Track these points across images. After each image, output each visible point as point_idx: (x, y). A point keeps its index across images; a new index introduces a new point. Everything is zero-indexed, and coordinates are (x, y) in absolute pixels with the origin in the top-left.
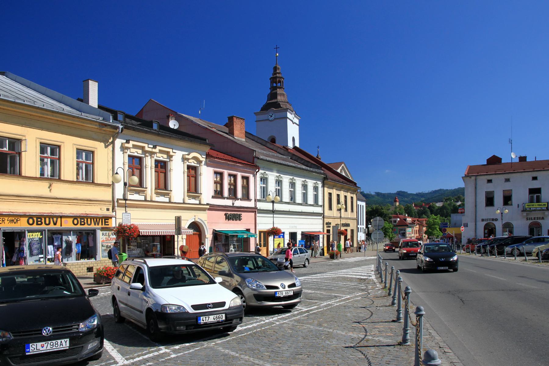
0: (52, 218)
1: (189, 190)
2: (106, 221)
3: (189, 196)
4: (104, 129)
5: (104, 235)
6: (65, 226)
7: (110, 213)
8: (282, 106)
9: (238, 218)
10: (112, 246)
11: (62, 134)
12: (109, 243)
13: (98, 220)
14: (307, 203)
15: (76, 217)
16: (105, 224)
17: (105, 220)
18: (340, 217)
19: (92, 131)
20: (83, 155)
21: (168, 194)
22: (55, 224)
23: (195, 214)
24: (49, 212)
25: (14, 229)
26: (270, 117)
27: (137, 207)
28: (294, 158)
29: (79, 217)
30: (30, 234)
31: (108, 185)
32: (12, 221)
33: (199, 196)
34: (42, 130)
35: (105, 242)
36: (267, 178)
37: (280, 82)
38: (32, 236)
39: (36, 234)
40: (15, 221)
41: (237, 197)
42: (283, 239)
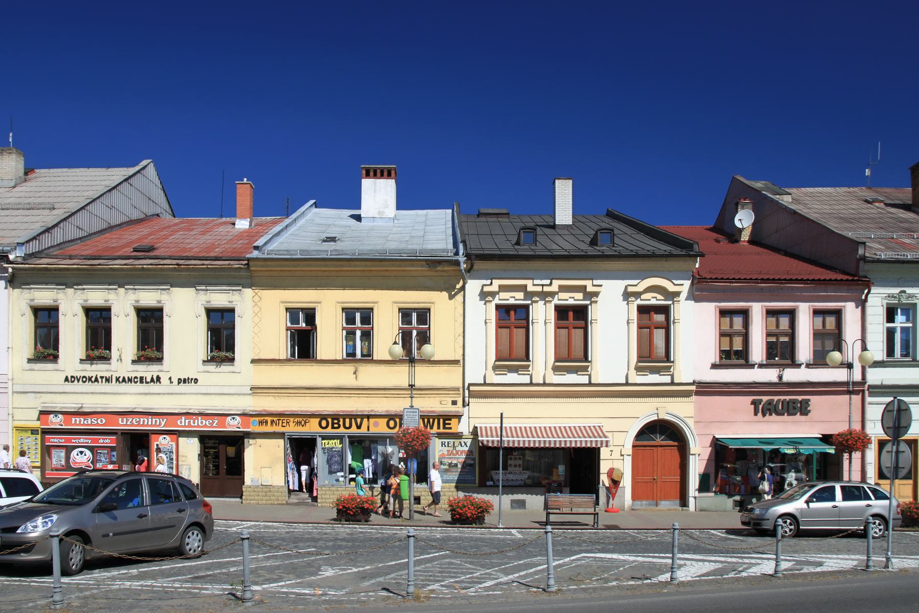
0: (354, 419)
1: (650, 357)
2: (447, 422)
3: (638, 369)
4: (439, 268)
5: (445, 446)
6: (373, 430)
7: (458, 408)
9: (795, 408)
10: (459, 464)
11: (375, 290)
13: (431, 420)
15: (393, 417)
16: (444, 428)
19: (424, 276)
21: (585, 369)
22: (359, 427)
23: (658, 405)
24: (355, 409)
25: (301, 434)
27: (513, 397)
30: (325, 441)
31: (456, 362)
32: (299, 423)
33: (670, 367)
34: (344, 290)
38: (328, 444)
39: (334, 441)
40: (303, 422)
41: (795, 361)
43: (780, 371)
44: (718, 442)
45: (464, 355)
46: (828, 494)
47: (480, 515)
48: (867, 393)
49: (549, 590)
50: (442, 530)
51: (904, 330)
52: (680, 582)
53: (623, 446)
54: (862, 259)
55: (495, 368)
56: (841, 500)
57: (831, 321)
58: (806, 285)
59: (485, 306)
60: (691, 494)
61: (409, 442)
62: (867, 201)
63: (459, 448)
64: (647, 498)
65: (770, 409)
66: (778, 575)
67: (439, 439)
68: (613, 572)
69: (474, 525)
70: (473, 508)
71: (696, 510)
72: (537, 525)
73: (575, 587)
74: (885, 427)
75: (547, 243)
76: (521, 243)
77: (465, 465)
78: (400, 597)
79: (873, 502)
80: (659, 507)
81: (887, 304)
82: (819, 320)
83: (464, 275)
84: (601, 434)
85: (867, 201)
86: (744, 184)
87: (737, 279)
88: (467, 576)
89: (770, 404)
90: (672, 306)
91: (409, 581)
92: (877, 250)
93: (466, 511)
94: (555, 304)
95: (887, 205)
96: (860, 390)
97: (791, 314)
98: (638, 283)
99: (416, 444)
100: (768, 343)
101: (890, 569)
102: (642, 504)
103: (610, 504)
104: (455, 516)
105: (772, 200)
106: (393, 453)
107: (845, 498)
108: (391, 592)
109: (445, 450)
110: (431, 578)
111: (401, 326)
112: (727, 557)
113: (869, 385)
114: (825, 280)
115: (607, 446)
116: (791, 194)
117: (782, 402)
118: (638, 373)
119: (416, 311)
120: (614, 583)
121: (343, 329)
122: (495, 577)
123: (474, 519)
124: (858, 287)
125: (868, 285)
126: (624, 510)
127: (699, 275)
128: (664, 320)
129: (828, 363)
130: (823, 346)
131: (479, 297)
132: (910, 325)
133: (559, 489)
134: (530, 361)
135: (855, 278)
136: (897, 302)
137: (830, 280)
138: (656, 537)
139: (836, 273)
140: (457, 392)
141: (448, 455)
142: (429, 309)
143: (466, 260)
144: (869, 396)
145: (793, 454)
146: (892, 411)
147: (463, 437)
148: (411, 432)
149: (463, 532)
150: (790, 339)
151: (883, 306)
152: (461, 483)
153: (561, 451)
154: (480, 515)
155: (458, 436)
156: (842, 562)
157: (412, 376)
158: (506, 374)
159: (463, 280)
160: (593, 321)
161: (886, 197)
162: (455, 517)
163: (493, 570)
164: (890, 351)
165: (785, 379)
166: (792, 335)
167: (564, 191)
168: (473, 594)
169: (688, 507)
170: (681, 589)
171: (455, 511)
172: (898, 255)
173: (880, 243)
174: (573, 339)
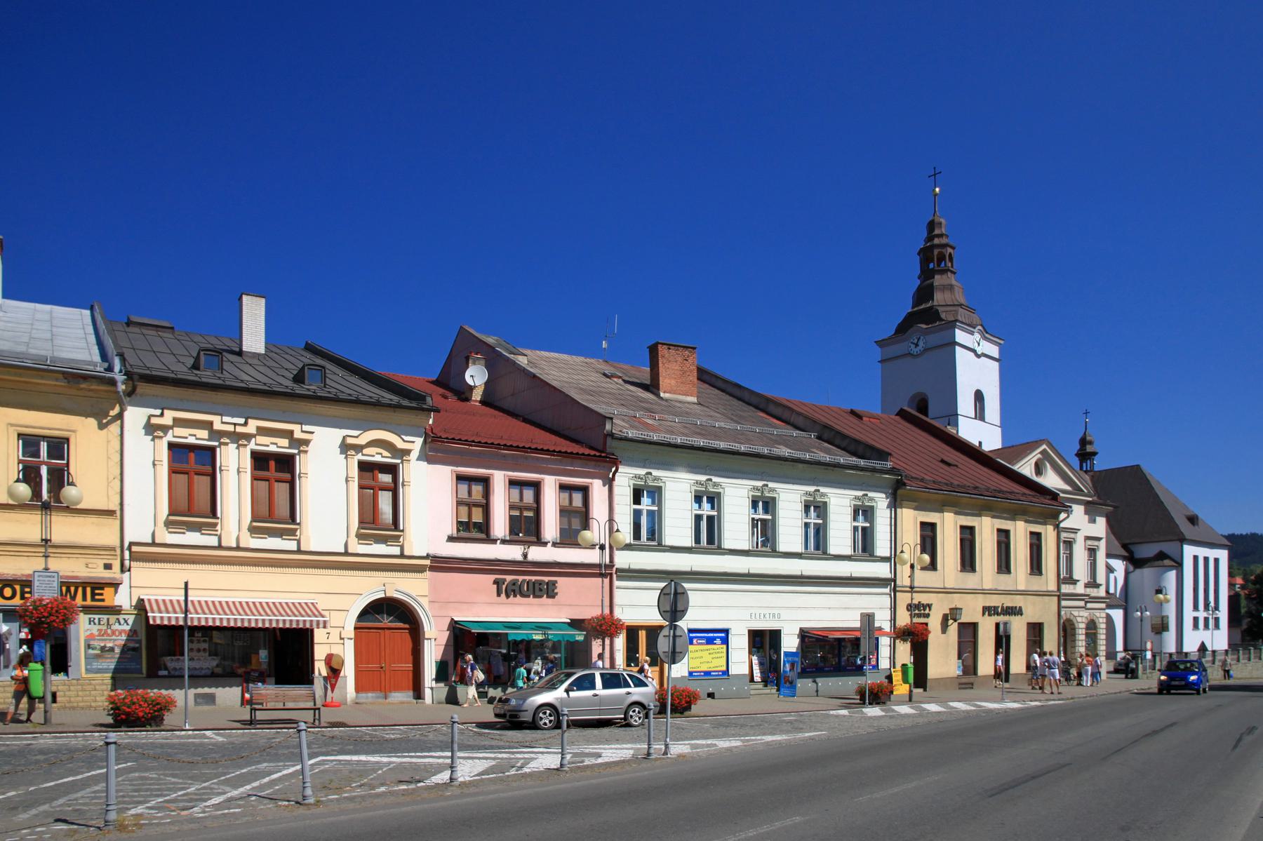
2: (97, 592)
3: (360, 536)
4: (83, 386)
7: (115, 573)
8: (943, 316)
9: (541, 590)
10: (116, 648)
12: (108, 641)
13: (73, 589)
14: (825, 553)
16: (93, 599)
17: (93, 590)
18: (912, 587)
20: (42, 446)
23: (386, 580)
26: (913, 346)
28: (826, 436)
29: (16, 581)
31: (110, 513)
33: (400, 536)
35: (98, 639)
36: (660, 488)
37: (941, 258)
41: (541, 539)
42: (725, 646)
43: (525, 549)
44: (458, 626)
45: (122, 504)
46: (586, 683)
47: (156, 713)
48: (615, 576)
49: (306, 802)
50: (101, 736)
51: (650, 513)
52: (461, 782)
53: (343, 628)
54: (610, 435)
55: (168, 524)
56: (601, 688)
57: (477, 489)
58: (552, 457)
59: (153, 442)
60: (426, 685)
61: (44, 617)
62: (605, 375)
63: (116, 627)
64: (373, 689)
65: (513, 591)
66: (564, 769)
67: (85, 614)
68: (372, 777)
69: (148, 728)
70: (146, 705)
71: (433, 703)
72: (238, 725)
73: (336, 797)
74: (661, 610)
75: (234, 372)
76: (202, 367)
77: (125, 649)
78: (92, 829)
79: (632, 690)
80: (389, 700)
81: (634, 484)
82: (464, 488)
83: (122, 399)
84: (317, 613)
85: (605, 375)
86: (474, 336)
87: (457, 440)
88: (180, 793)
89: (514, 584)
90: (401, 465)
91: (108, 805)
92: (620, 427)
93: (137, 709)
94: (251, 449)
95: (626, 382)
96: (609, 573)
97: (536, 486)
98: (361, 434)
99: (54, 621)
100: (511, 517)
101: (669, 756)
102: (369, 696)
103: (328, 697)
104: (119, 716)
105: (508, 359)
106: (9, 633)
107: (605, 686)
108: (73, 823)
109: (95, 629)
110: (126, 799)
111: (21, 457)
112: (495, 753)
113: (617, 569)
114: (572, 453)
115: (325, 627)
116: (526, 356)
117: (528, 582)
118: (360, 542)
119: (46, 439)
120: (383, 789)
121: (20, 462)
122: (220, 791)
123: (146, 719)
124: (606, 464)
125: (615, 462)
126: (346, 704)
127: (432, 433)
128: (391, 481)
129: (580, 543)
130: (570, 523)
131: (144, 430)
132: (656, 508)
133: (262, 678)
134: (218, 518)
135: (603, 455)
136: (643, 483)
137: (577, 454)
138: (401, 734)
139: (583, 447)
140: (112, 553)
141: (99, 635)
142: (68, 440)
143: (125, 380)
144: (617, 580)
145: (541, 640)
146: (669, 594)
147: (123, 612)
148: (48, 604)
149: (136, 737)
150: (534, 514)
151: (629, 486)
152: (118, 673)
153: (262, 634)
154: (156, 713)
155: (116, 610)
156: (618, 751)
157: (46, 527)
158: (184, 533)
159: (120, 405)
160: (302, 475)
161: (624, 373)
162: (119, 718)
163: (213, 783)
164: (637, 535)
165: (530, 558)
166: (486, 509)
167: (254, 313)
168: (201, 815)
169: (424, 699)
170: (466, 791)
171: (119, 710)
172: (664, 437)
173: (623, 420)
174: (276, 492)
